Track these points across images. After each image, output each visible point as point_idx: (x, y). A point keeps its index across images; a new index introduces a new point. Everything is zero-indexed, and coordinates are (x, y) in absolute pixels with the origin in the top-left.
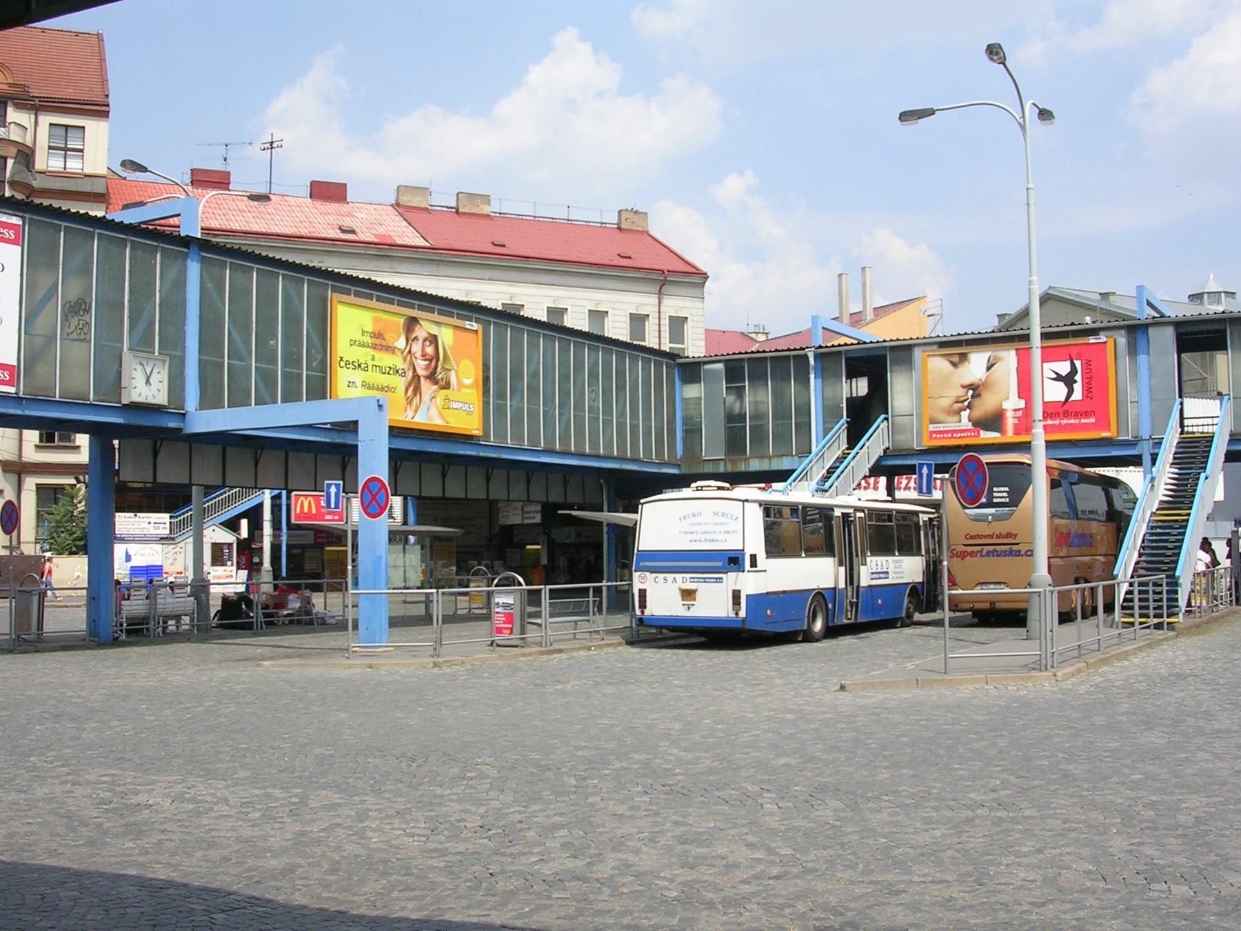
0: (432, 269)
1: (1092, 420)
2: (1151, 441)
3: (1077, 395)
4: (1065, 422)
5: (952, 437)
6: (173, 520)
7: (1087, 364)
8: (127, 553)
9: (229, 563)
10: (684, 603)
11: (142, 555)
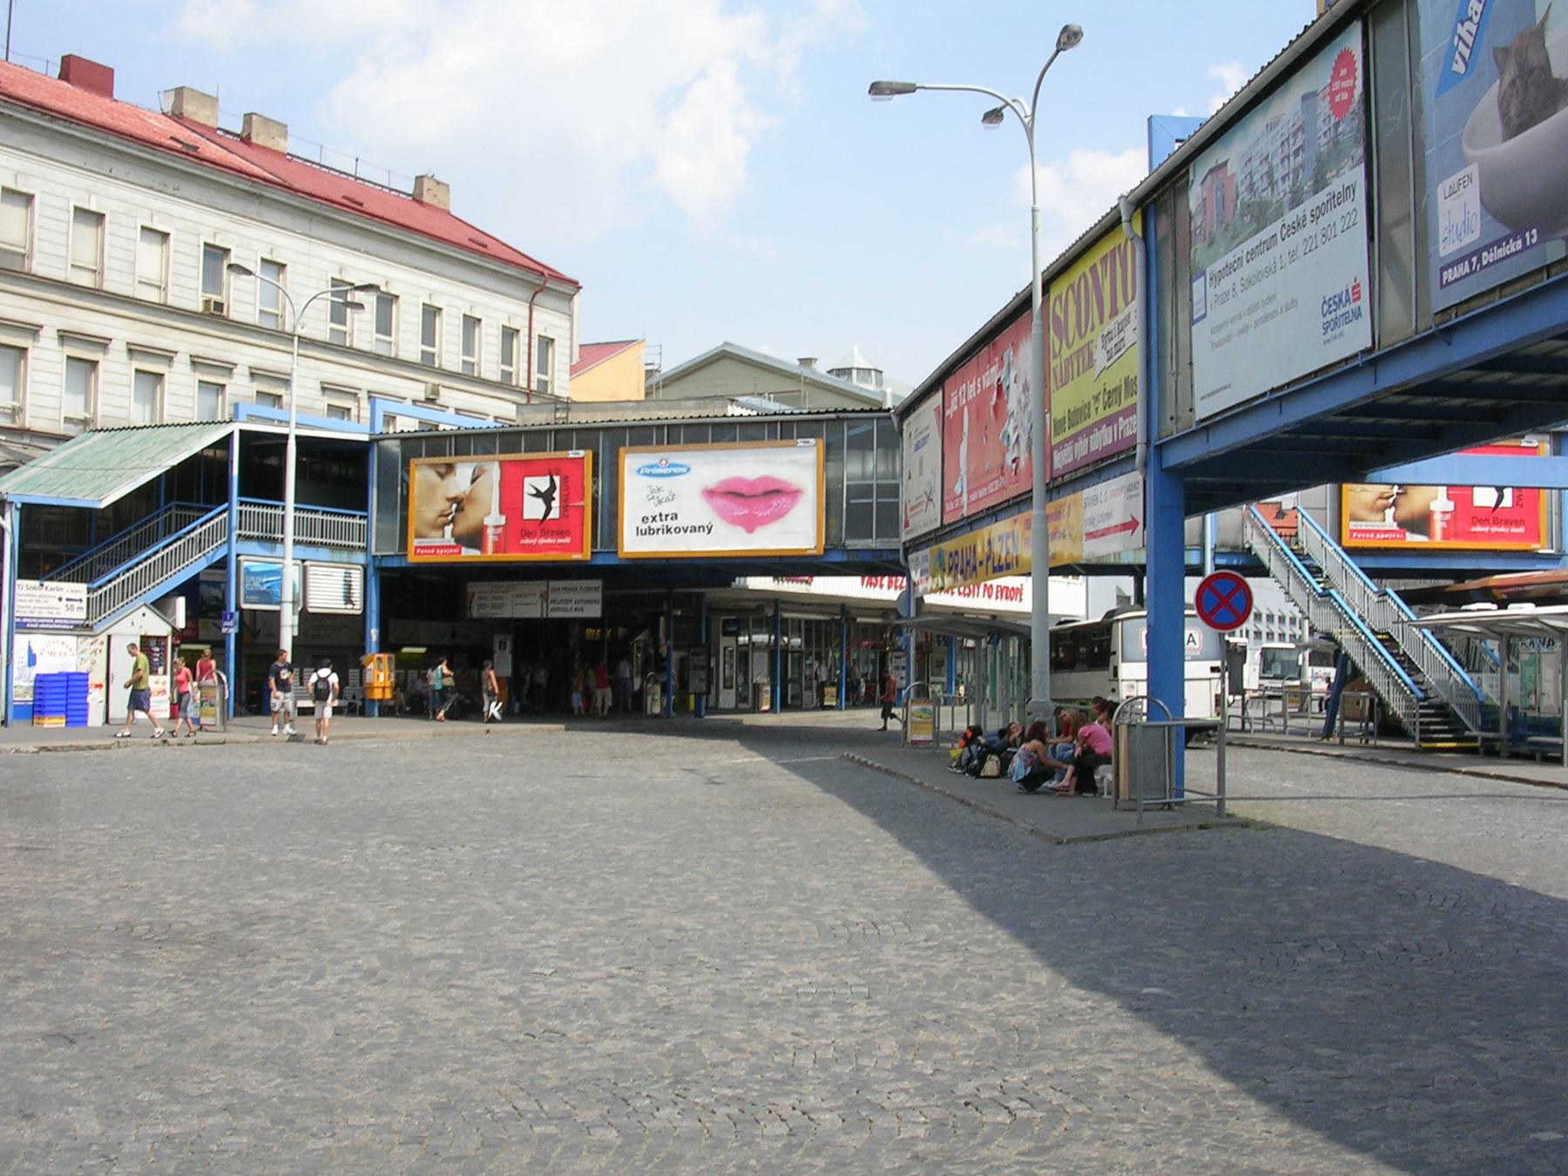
0: (301, 224)
1: (1521, 530)
3: (554, 514)
4: (1494, 529)
5: (1374, 538)
6: (91, 596)
7: (564, 481)
8: (30, 650)
9: (161, 670)
11: (51, 654)
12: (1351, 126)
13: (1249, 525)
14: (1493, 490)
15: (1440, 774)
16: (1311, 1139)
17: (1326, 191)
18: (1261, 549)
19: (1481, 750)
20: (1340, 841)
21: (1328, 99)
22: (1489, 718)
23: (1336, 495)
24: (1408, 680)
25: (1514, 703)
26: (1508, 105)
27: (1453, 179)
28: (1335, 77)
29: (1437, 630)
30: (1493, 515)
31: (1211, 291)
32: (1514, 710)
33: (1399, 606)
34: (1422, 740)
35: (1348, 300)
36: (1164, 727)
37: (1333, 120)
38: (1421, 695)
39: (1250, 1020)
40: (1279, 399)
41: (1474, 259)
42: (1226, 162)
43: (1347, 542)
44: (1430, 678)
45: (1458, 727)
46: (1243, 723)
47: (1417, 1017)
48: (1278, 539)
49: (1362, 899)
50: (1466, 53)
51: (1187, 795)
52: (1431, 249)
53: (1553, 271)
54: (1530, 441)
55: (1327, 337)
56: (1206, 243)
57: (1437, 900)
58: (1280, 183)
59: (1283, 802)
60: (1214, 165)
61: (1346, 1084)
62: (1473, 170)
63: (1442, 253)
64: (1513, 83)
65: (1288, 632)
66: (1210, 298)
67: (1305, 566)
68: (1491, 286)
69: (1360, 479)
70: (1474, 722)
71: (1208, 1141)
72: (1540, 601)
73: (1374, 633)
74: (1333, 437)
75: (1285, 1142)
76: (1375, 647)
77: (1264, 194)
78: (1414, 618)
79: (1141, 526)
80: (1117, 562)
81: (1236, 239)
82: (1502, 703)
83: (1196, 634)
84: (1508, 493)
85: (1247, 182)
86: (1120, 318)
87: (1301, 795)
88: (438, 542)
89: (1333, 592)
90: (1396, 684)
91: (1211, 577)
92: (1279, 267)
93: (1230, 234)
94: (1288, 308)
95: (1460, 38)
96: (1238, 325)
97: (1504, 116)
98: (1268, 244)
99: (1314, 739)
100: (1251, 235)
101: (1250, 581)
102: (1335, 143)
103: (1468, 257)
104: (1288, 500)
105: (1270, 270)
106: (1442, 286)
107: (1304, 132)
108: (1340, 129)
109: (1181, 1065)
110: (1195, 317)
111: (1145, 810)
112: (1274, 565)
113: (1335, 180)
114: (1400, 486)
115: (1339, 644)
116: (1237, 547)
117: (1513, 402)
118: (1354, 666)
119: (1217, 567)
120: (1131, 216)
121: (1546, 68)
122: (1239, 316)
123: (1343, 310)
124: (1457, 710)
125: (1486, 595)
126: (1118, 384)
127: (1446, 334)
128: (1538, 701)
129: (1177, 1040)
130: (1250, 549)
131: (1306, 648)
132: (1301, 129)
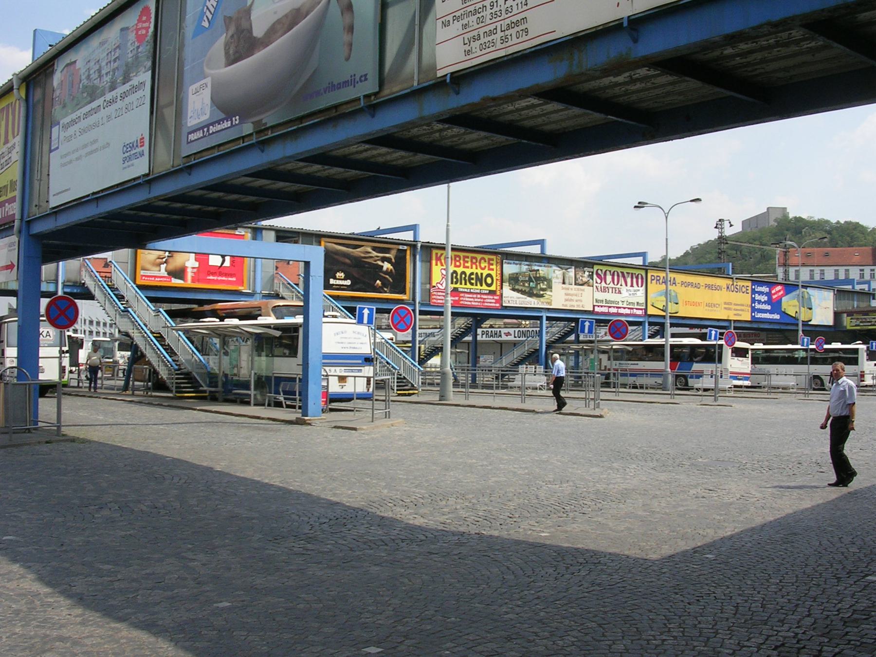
1: (234, 279)
2: (261, 295)
4: (220, 278)
10: (340, 384)
12: (146, 48)
13: (83, 269)
14: (220, 257)
15: (186, 411)
16: (93, 616)
17: (130, 83)
18: (90, 283)
19: (209, 397)
20: (126, 448)
21: (135, 32)
22: (214, 380)
23: (134, 255)
24: (170, 359)
25: (226, 372)
26: (229, 48)
27: (198, 85)
28: (140, 20)
29: (186, 332)
30: (219, 270)
31: (62, 134)
32: (226, 376)
33: (166, 318)
34: (177, 392)
35: (137, 146)
36: (26, 384)
37: (137, 44)
38: (176, 367)
39: (66, 551)
40: (97, 198)
41: (205, 130)
42: (75, 62)
43: (139, 282)
44: (182, 358)
45: (196, 385)
46: (79, 383)
47: (159, 544)
48: (100, 279)
49: (134, 480)
50: (210, 17)
51: (40, 424)
52: (183, 122)
53: (246, 140)
54: (240, 231)
55: (125, 165)
56: (61, 106)
57: (176, 480)
58: (105, 76)
59: (96, 427)
60: (69, 62)
61: (116, 584)
62: (208, 81)
63: (189, 125)
64: (232, 36)
65: (108, 332)
66: (62, 138)
67: (114, 294)
68: (213, 145)
69: (143, 247)
70: (205, 382)
71: (34, 623)
72: (242, 318)
73: (152, 333)
74: (128, 222)
75: (79, 619)
76: (152, 341)
77: (95, 82)
78: (174, 325)
79: (16, 268)
80: (6, 288)
81: (78, 106)
82: (220, 372)
83: (48, 332)
84: (228, 259)
85: (87, 74)
86: (9, 145)
87: (107, 423)
88: (156, 273)
89: (130, 309)
90: (163, 361)
91: (60, 297)
92: (101, 124)
93: (75, 102)
94: (104, 147)
95: (208, 8)
96: (76, 155)
97: (227, 53)
98: (96, 110)
99: (118, 392)
100: (86, 104)
101: (79, 302)
102: (136, 57)
103: (202, 128)
104: (108, 255)
105: (96, 125)
106: (188, 143)
107: (120, 49)
108: (139, 50)
109: (22, 580)
110: (52, 148)
111: (14, 433)
112: (97, 293)
113: (135, 78)
114: (170, 252)
115: (132, 339)
116: (76, 282)
117: (225, 209)
118: (142, 353)
119: (65, 293)
120: (19, 86)
121: (250, 31)
122: (77, 150)
123: (134, 151)
124: (196, 376)
125: (214, 313)
126: (6, 184)
127: (189, 169)
128: (239, 371)
129: (21, 566)
130: (84, 284)
131: (116, 340)
132: (118, 47)
